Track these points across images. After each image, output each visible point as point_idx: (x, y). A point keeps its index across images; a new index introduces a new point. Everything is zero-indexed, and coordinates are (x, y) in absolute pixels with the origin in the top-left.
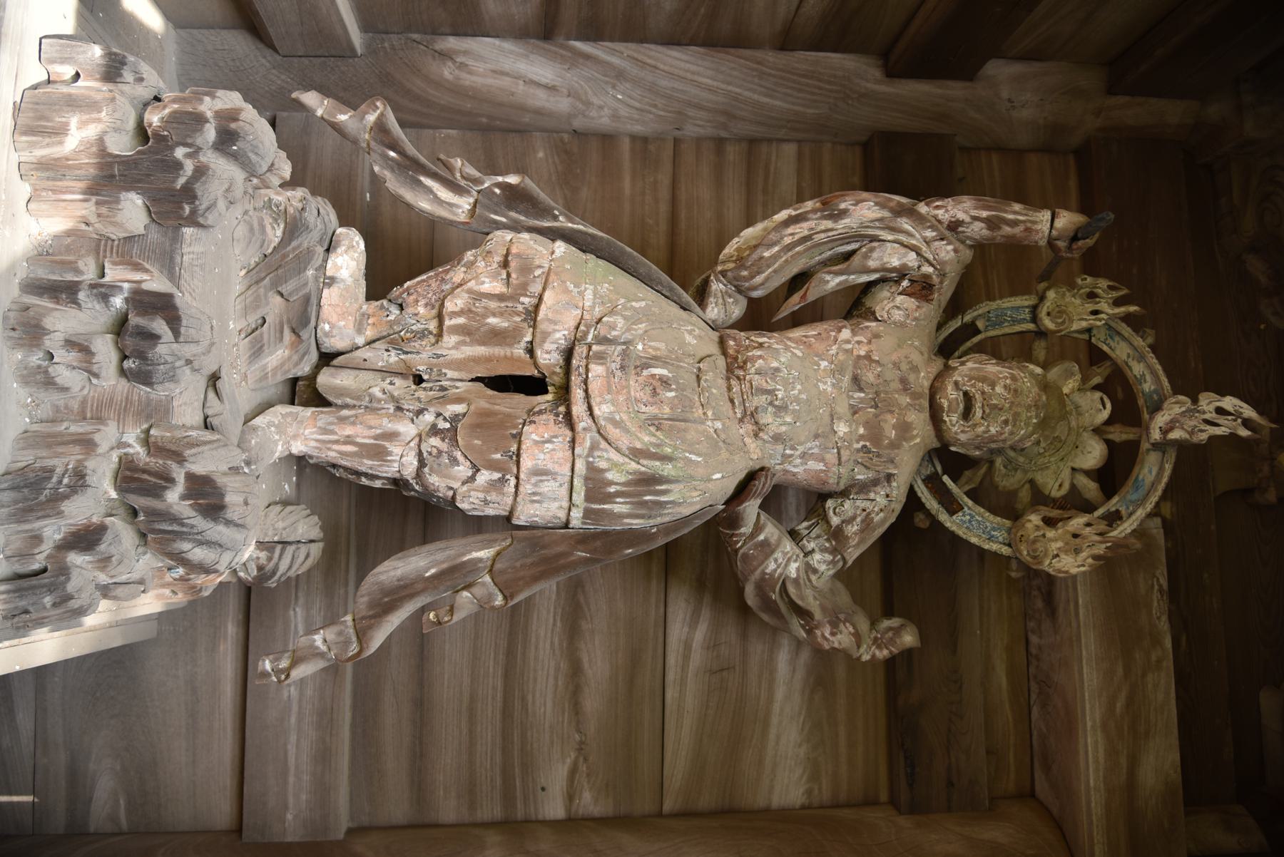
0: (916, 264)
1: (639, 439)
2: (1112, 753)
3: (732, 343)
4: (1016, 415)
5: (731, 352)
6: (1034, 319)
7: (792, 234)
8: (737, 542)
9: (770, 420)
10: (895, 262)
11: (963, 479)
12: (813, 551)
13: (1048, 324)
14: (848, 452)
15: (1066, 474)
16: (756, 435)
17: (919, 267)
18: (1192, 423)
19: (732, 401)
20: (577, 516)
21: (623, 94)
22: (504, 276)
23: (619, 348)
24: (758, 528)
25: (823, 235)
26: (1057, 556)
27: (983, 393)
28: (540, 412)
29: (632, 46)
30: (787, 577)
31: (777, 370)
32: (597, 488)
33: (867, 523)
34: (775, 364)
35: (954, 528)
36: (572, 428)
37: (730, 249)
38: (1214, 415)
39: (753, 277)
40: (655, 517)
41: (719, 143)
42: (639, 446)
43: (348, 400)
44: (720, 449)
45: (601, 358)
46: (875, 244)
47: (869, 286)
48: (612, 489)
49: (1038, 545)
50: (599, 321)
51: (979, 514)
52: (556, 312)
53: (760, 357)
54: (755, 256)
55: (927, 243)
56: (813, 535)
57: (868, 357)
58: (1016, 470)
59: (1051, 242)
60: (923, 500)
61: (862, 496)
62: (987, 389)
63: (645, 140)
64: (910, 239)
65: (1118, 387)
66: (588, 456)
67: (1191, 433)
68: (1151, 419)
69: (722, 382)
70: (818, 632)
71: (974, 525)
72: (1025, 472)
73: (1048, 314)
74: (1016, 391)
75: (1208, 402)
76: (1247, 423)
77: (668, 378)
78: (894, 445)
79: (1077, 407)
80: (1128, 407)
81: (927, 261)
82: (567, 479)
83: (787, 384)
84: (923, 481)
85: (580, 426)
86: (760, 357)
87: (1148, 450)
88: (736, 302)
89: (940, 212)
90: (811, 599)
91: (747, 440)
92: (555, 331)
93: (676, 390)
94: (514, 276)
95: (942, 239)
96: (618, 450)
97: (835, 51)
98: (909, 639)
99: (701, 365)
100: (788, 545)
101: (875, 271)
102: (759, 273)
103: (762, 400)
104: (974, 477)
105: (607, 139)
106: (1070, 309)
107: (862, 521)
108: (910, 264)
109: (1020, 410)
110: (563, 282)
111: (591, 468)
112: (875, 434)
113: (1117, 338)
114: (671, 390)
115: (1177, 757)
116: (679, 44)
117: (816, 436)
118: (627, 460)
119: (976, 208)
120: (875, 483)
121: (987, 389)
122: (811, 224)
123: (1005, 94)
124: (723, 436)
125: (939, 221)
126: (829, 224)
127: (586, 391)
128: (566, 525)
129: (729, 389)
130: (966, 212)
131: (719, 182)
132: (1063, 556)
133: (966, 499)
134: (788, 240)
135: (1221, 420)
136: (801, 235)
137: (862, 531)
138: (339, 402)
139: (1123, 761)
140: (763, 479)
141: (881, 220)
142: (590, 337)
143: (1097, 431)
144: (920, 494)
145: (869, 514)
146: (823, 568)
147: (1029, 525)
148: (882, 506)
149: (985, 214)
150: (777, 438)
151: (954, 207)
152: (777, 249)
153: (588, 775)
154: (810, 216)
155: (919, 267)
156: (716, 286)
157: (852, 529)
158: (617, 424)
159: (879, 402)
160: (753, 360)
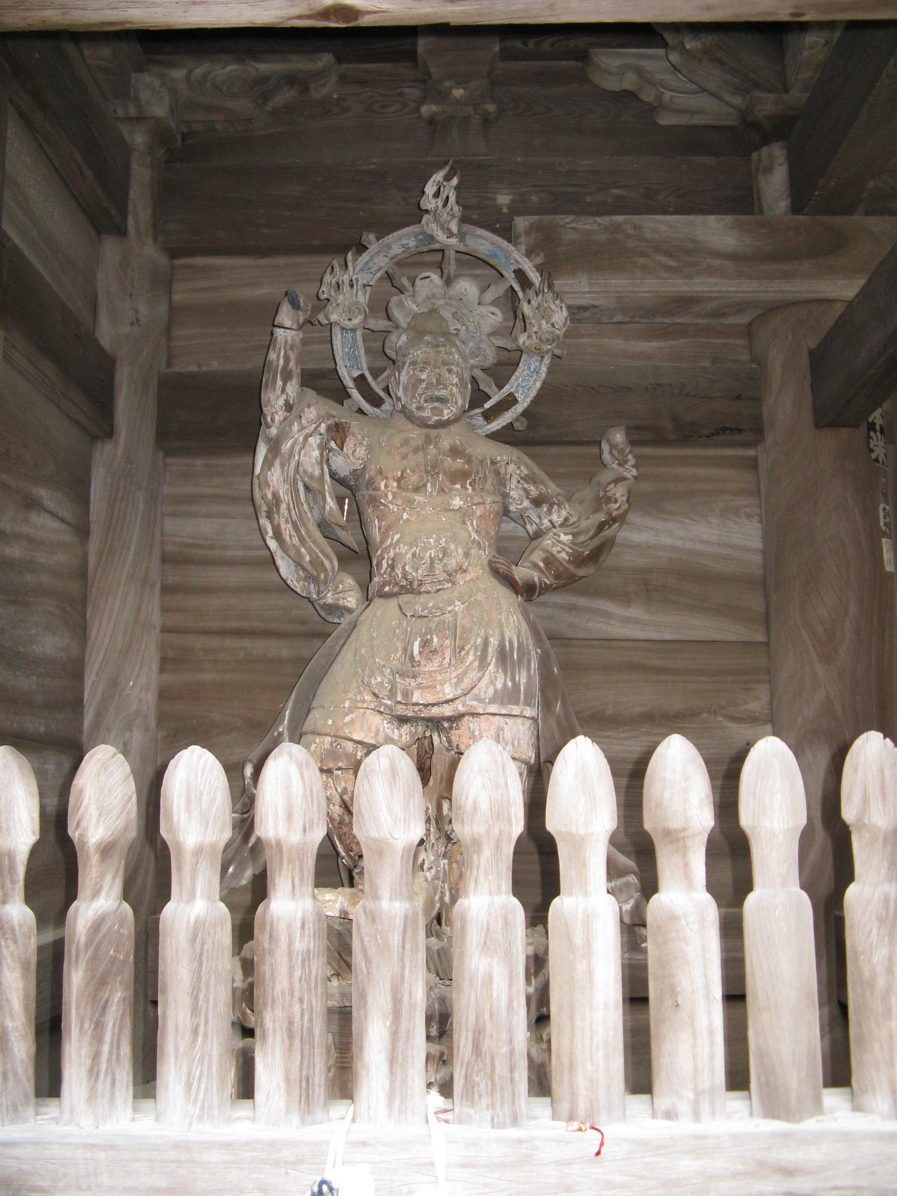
0: (318, 437)
1: (471, 663)
2: (710, 271)
3: (387, 589)
4: (445, 363)
5: (396, 589)
6: (354, 330)
7: (290, 537)
8: (545, 583)
9: (454, 561)
10: (316, 453)
11: (487, 390)
12: (550, 521)
13: (357, 321)
14: (476, 498)
15: (483, 310)
16: (465, 571)
17: (321, 434)
18: (445, 215)
19: (438, 590)
20: (529, 712)
21: (129, 680)
22: (340, 772)
23: (398, 680)
24: (535, 566)
25: (293, 512)
26: (552, 324)
27: (426, 388)
28: (449, 741)
29: (87, 672)
30: (572, 543)
31: (414, 555)
32: (510, 696)
33: (530, 479)
34: (409, 555)
35: (529, 400)
36: (462, 716)
37: (298, 587)
38: (439, 200)
39: (326, 570)
40: (529, 650)
41: (166, 590)
42: (476, 664)
43: (437, 898)
44: (475, 600)
45: (407, 694)
46: (301, 469)
47: (333, 475)
48: (509, 684)
49: (543, 337)
50: (375, 694)
51: (517, 379)
52: (369, 729)
53: (403, 568)
54: (309, 568)
55: (302, 428)
56: (537, 521)
57: (398, 480)
58: (479, 348)
59: (300, 327)
60: (505, 424)
61: (508, 483)
62: (424, 385)
63: (164, 660)
64: (297, 444)
65: (412, 263)
66: (484, 703)
67: (453, 216)
68: (439, 242)
69: (422, 598)
70: (614, 513)
71: (526, 384)
72: (481, 341)
73: (350, 320)
74: (425, 363)
75: (429, 202)
76: (448, 178)
77: (422, 641)
78: (469, 461)
79: (428, 298)
80: (432, 257)
81: (316, 429)
82: (501, 719)
83: (425, 549)
84: (488, 424)
85: (461, 709)
86: (403, 568)
87: (465, 245)
88: (342, 582)
89: (277, 418)
90: (589, 522)
91: (468, 578)
92: (384, 731)
93: (431, 635)
94: (340, 764)
95: (300, 417)
96: (480, 679)
97: (89, 486)
98: (619, 437)
99: (409, 615)
100: (547, 542)
101: (322, 470)
102: (323, 564)
103: (439, 567)
104: (487, 384)
105: (165, 695)
106: (347, 303)
107: (527, 483)
108: (318, 441)
109: (440, 360)
110: (344, 724)
111: (493, 701)
112: (459, 476)
113: (371, 264)
114: (432, 639)
115: (712, 218)
116: (85, 629)
117: (464, 523)
118: (488, 672)
119: (275, 390)
120: (497, 473)
121: (424, 385)
122: (282, 522)
123: (126, 329)
124: (466, 598)
125: (285, 419)
126: (283, 507)
127: (433, 705)
128: (534, 720)
129: (428, 592)
130: (278, 398)
131: (204, 590)
132: (553, 321)
133: (504, 390)
134: (296, 541)
135: (443, 196)
136: (292, 529)
137: (535, 483)
138: (438, 905)
139: (717, 262)
140: (497, 565)
141: (282, 465)
142: (389, 702)
143: (448, 282)
144: (500, 427)
145: (522, 478)
146: (564, 513)
147: (528, 343)
148: (513, 464)
149: (280, 383)
150: (467, 555)
151: (272, 407)
152: (303, 550)
153: (736, 706)
154: (276, 522)
155: (321, 434)
156: (330, 598)
157: (534, 491)
158: (460, 679)
159: (432, 469)
160: (405, 575)
